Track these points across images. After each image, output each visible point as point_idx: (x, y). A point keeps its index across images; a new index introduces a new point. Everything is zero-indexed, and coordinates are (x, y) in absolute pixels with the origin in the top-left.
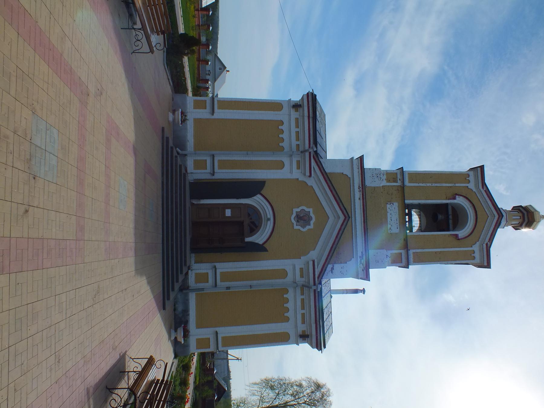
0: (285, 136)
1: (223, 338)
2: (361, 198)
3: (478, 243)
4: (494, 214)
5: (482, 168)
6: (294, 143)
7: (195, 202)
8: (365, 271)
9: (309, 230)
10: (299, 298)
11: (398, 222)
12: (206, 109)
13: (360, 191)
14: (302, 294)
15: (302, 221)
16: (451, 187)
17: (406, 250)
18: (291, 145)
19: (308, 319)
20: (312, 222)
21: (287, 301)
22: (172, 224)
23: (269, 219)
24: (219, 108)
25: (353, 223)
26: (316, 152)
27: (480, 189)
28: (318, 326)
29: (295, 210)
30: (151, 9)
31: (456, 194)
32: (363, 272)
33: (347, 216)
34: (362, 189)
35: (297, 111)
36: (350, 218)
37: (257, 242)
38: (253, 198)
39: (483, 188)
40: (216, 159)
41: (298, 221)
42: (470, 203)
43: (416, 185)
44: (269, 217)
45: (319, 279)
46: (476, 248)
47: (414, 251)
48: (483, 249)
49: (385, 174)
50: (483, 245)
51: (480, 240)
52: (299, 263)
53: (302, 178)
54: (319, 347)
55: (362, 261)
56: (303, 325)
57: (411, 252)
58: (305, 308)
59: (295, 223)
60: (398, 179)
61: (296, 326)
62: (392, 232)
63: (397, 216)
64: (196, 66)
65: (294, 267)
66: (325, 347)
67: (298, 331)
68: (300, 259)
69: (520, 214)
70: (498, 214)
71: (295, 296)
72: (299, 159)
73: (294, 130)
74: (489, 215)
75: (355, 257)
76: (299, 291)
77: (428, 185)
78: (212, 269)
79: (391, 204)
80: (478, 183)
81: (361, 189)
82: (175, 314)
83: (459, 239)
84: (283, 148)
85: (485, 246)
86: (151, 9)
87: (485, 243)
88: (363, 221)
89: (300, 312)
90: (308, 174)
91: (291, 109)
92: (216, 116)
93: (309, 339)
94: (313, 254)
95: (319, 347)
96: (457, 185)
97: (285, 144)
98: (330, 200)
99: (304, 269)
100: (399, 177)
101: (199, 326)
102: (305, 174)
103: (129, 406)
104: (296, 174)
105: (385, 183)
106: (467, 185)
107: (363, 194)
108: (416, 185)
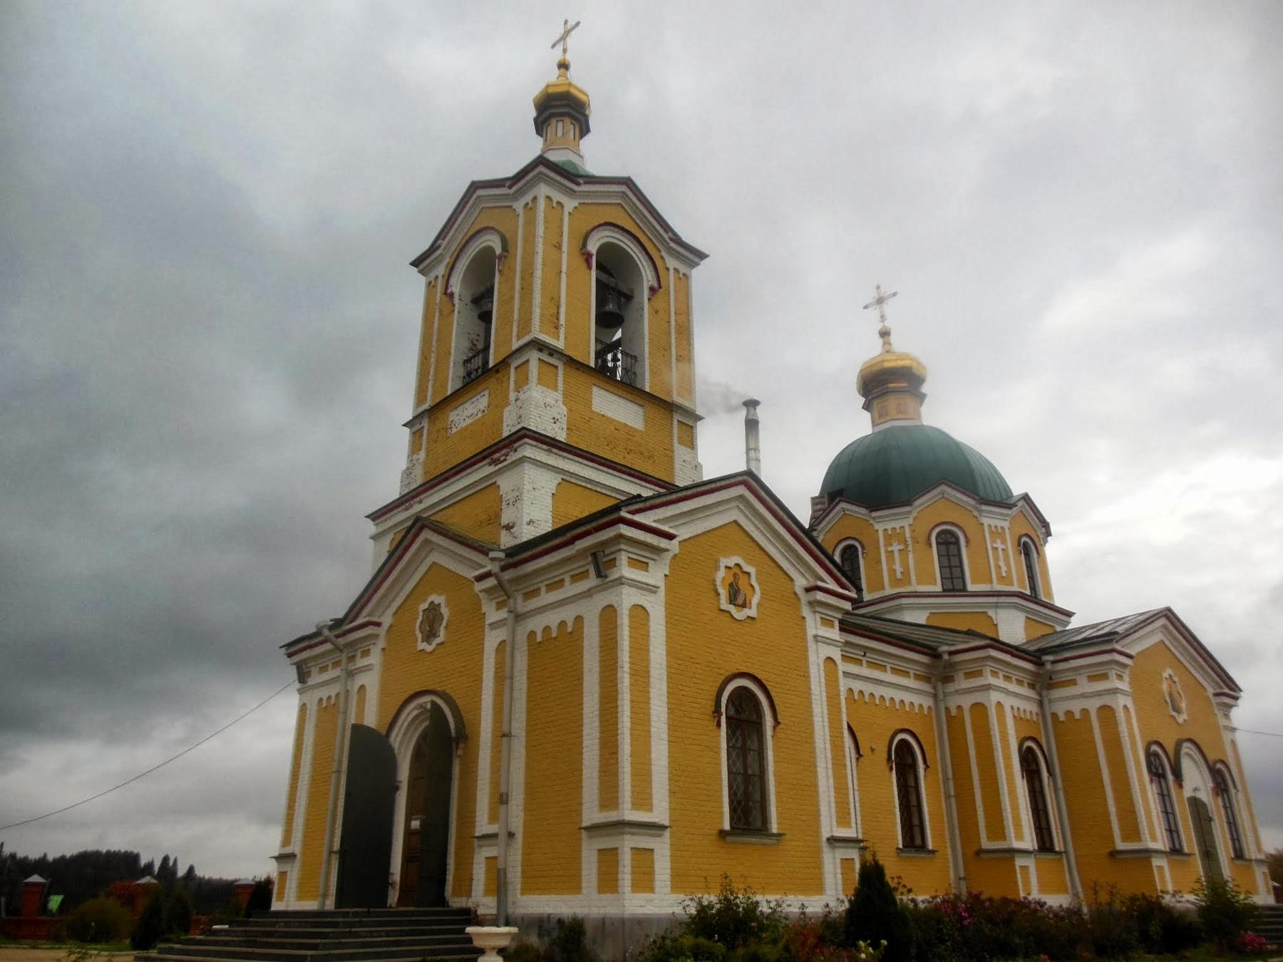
3: (663, 254)
4: (476, 200)
5: (415, 263)
8: (516, 445)
9: (448, 605)
13: (411, 506)
17: (509, 361)
22: (439, 942)
26: (331, 628)
27: (444, 250)
29: (725, 604)
31: (445, 293)
34: (406, 501)
35: (309, 674)
38: (399, 749)
39: (439, 247)
42: (460, 258)
50: (513, 195)
53: (381, 643)
59: (438, 640)
69: (553, 121)
70: (474, 192)
72: (520, 598)
74: (619, 201)
85: (672, 244)
88: (445, 484)
90: (369, 630)
91: (608, 579)
92: (660, 812)
99: (497, 600)
100: (417, 427)
102: (377, 636)
105: (422, 455)
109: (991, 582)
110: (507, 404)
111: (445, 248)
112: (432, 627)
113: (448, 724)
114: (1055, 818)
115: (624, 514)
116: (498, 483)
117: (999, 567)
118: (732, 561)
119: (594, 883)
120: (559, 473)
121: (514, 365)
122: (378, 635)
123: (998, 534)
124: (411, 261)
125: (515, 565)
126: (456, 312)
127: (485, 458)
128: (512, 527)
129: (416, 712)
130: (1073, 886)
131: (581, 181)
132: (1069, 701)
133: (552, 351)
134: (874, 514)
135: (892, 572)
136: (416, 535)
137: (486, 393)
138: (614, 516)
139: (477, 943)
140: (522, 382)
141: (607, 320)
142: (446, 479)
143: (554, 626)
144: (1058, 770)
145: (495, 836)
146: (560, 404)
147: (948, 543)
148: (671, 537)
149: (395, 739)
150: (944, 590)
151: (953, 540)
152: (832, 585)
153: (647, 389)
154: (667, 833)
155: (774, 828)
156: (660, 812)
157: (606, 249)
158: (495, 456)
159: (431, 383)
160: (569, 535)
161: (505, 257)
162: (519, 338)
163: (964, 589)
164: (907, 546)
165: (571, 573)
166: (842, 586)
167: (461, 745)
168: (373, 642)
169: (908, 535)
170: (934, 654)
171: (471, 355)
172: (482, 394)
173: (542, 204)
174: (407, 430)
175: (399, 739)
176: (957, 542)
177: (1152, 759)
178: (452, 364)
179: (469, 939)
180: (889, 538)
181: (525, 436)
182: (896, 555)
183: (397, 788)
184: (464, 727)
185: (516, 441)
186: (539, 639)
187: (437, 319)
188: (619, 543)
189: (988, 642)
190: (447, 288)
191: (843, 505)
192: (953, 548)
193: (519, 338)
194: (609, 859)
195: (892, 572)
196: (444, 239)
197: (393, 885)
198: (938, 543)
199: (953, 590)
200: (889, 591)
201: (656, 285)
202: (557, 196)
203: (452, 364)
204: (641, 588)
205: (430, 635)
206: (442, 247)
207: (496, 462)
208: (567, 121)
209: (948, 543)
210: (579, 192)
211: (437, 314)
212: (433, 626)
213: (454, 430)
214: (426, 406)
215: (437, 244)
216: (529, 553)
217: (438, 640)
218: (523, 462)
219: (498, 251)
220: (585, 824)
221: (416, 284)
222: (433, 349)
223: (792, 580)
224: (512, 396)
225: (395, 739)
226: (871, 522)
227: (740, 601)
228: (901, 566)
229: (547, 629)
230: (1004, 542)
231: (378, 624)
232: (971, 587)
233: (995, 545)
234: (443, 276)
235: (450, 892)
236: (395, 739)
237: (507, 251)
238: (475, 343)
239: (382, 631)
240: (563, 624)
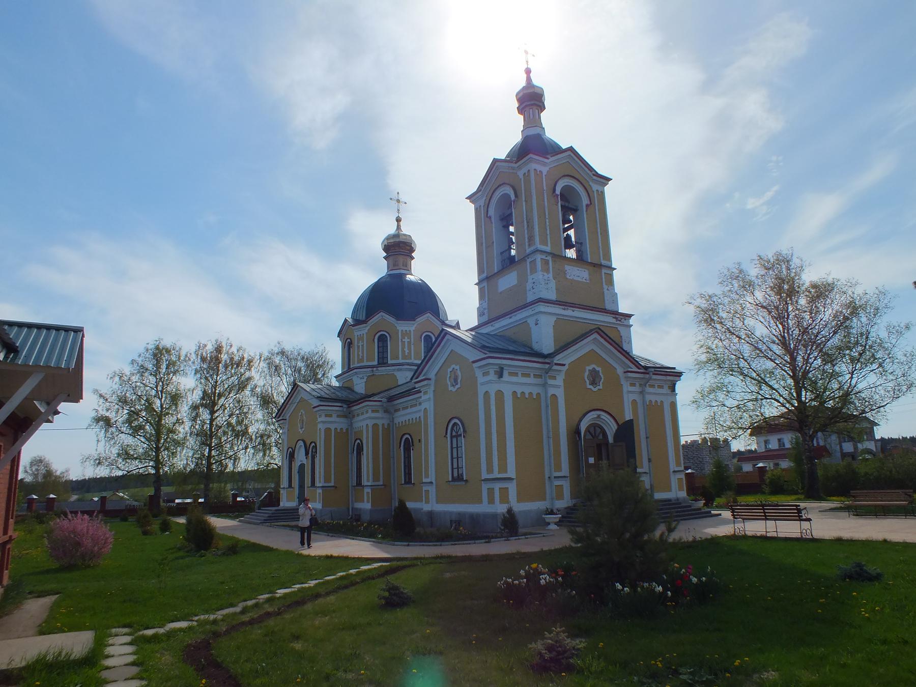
0: (527, 391)
2: (574, 309)
3: (591, 183)
6: (531, 380)
11: (580, 269)
12: (508, 488)
18: (530, 384)
20: (597, 369)
23: (599, 416)
24: (506, 472)
25: (593, 323)
28: (671, 374)
30: (769, 516)
32: (575, 312)
33: (595, 331)
34: (566, 306)
36: (601, 327)
37: (614, 430)
40: (424, 480)
41: (596, 384)
43: (549, 237)
44: (595, 416)
45: (640, 367)
46: (595, 187)
47: (527, 247)
49: (542, 273)
52: (626, 387)
53: (432, 388)
54: (681, 374)
56: (557, 378)
57: (604, 262)
60: (546, 258)
61: (667, 394)
62: (588, 279)
63: (576, 268)
64: (130, 523)
65: (629, 392)
66: (674, 368)
67: (494, 379)
68: (622, 385)
73: (520, 379)
75: (616, 326)
77: (548, 224)
78: (675, 475)
79: (566, 272)
81: (566, 307)
83: (591, 204)
84: (538, 394)
85: (594, 177)
86: (769, 516)
87: (592, 176)
88: (591, 312)
90: (425, 382)
92: (513, 476)
93: (505, 368)
94: (620, 371)
95: (681, 374)
96: (545, 188)
97: (535, 391)
100: (482, 286)
103: (79, 686)
104: (560, 381)
105: (551, 275)
106: (544, 177)
108: (549, 237)
114: (320, 475)
116: (528, 322)
118: (590, 368)
119: (434, 499)
121: (529, 261)
122: (430, 384)
123: (406, 334)
128: (428, 338)
132: (402, 417)
134: (399, 322)
135: (403, 351)
140: (534, 270)
143: (659, 402)
147: (382, 340)
153: (589, 261)
154: (515, 481)
156: (511, 472)
158: (617, 316)
162: (547, 246)
168: (558, 373)
173: (532, 174)
180: (404, 335)
182: (406, 343)
191: (382, 313)
194: (491, 492)
195: (403, 351)
196: (482, 187)
200: (401, 361)
201: (589, 203)
202: (539, 167)
208: (535, 107)
214: (485, 275)
219: (513, 197)
220: (483, 478)
221: (471, 207)
223: (616, 369)
226: (396, 325)
228: (408, 350)
230: (363, 342)
231: (430, 379)
233: (403, 340)
234: (484, 206)
239: (432, 382)
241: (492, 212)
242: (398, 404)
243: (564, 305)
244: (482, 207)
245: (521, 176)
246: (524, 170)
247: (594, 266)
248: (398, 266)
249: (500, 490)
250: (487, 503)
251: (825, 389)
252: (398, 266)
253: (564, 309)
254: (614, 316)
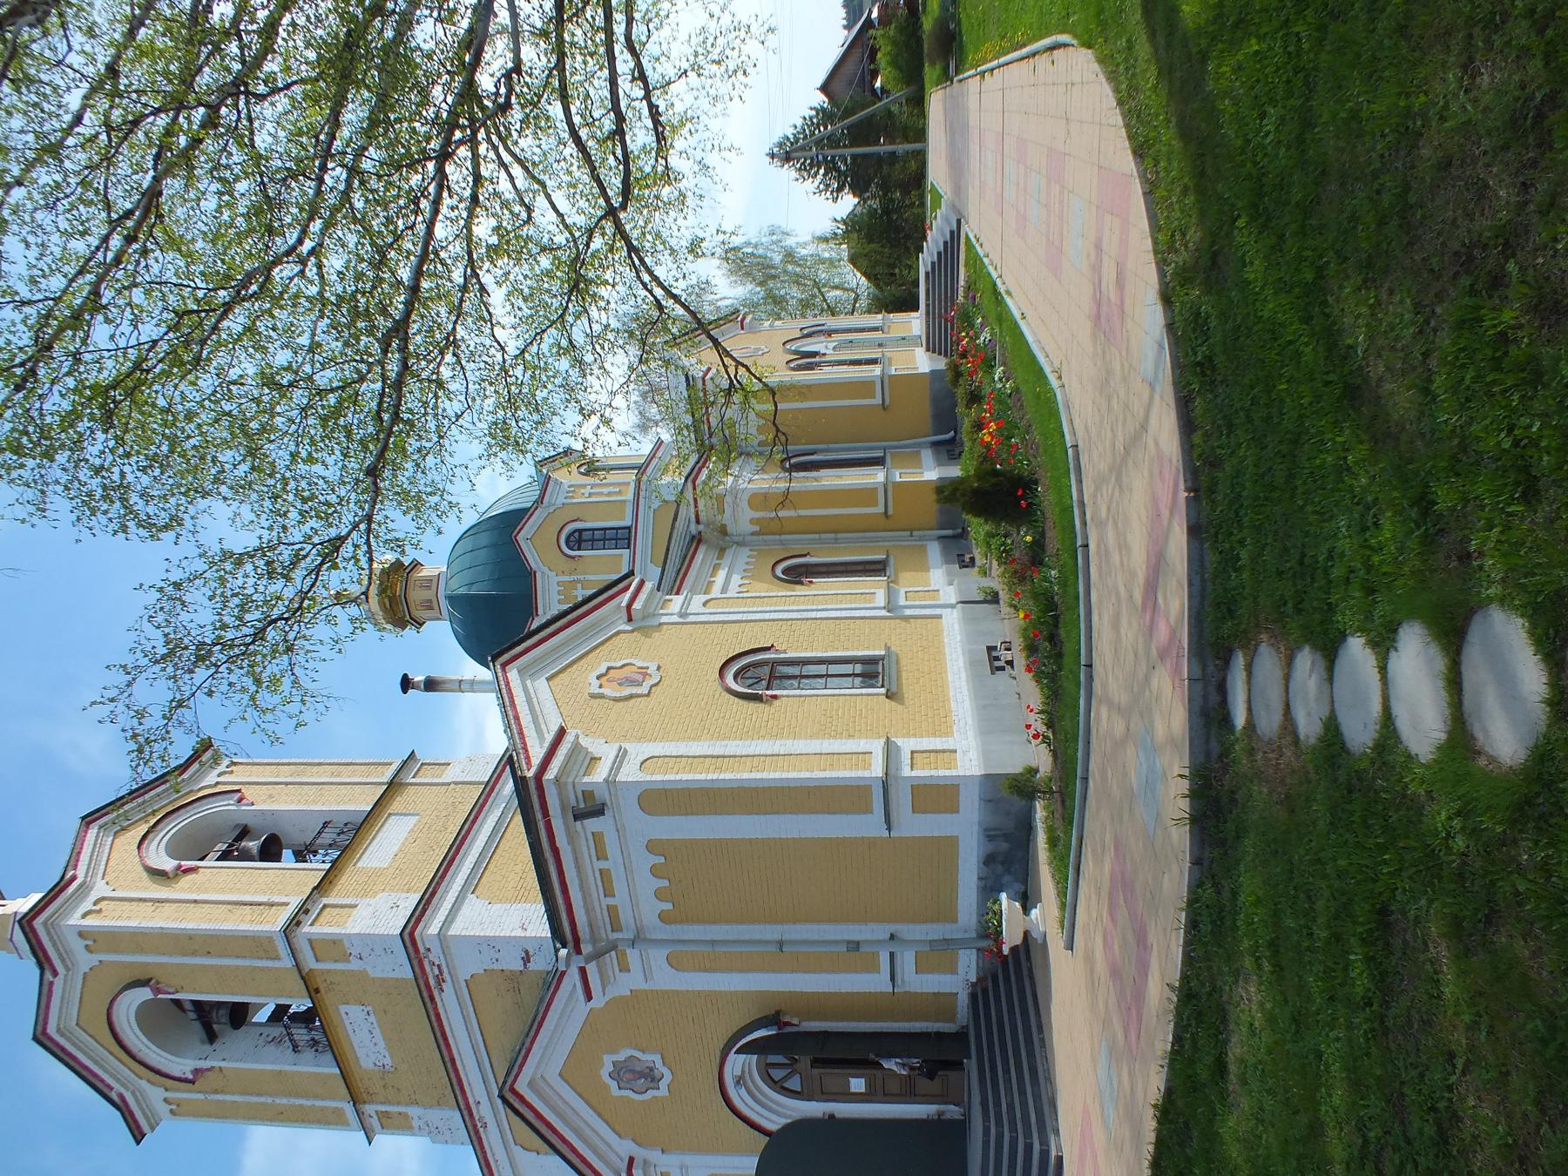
1: (868, 810)
4: (62, 1035)
7: (953, 1111)
8: (422, 950)
9: (606, 1087)
10: (620, 899)
11: (349, 1028)
14: (612, 911)
15: (638, 1069)
16: (216, 1092)
19: (584, 849)
21: (659, 895)
27: (127, 1089)
31: (192, 1082)
34: (475, 1126)
38: (785, 1117)
39: (121, 1097)
47: (277, 964)
48: (63, 961)
50: (68, 969)
51: (81, 977)
53: (654, 1156)
55: (437, 972)
58: (598, 875)
59: (659, 1064)
63: (355, 1040)
71: (634, 905)
76: (625, 916)
80: (137, 1100)
81: (479, 1125)
82: (1025, 882)
89: (614, 863)
91: (608, 802)
98: (576, 860)
99: (617, 970)
100: (375, 1122)
101: (951, 843)
105: (413, 1111)
107: (471, 1115)
108: (319, 1103)
109: (625, 501)
110: (364, 973)
111: (123, 1085)
112: (642, 1075)
113: (762, 1038)
115: (530, 774)
117: (609, 494)
120: (464, 898)
124: (134, 1143)
125: (577, 941)
126: (223, 1064)
127: (432, 998)
128: (527, 952)
129: (743, 1091)
130: (914, 445)
131: (70, 874)
133: (303, 909)
136: (521, 1098)
137: (343, 1009)
138: (532, 786)
139: (1018, 940)
141: (271, 851)
142: (453, 1060)
144: (812, 447)
145: (892, 955)
146: (372, 901)
147: (579, 539)
148: (562, 733)
149: (774, 1123)
150: (629, 547)
151: (577, 534)
152: (627, 596)
155: (883, 653)
157: (173, 852)
158: (432, 982)
159: (319, 1103)
160: (548, 854)
161: (158, 983)
162: (277, 958)
163: (629, 528)
164: (579, 581)
165: (594, 859)
166: (627, 588)
167: (787, 1019)
169: (567, 578)
170: (697, 540)
171: (288, 1043)
172: (344, 1016)
174: (379, 1139)
175: (774, 1117)
176: (580, 531)
177: (799, 368)
178: (295, 1068)
179: (1014, 949)
181: (412, 934)
183: (832, 1117)
184: (766, 1017)
185: (417, 950)
186: (668, 906)
187: (228, 1098)
188: (566, 783)
189: (690, 485)
190: (186, 1081)
192: (586, 535)
193: (277, 958)
197: (940, 1114)
198: (579, 549)
199: (629, 539)
203: (295, 1068)
204: (621, 763)
205: (651, 1077)
206: (122, 1090)
207: (440, 980)
209: (579, 539)
210: (86, 877)
211: (220, 1097)
212: (639, 1072)
213: (388, 1061)
214: (348, 1108)
215: (116, 1099)
216: (564, 916)
217: (659, 1064)
218: (445, 936)
219: (145, 994)
222: (269, 1100)
224: (355, 965)
225: (774, 1122)
227: (640, 678)
229: (659, 895)
232: (627, 522)
235: (951, 1025)
236: (774, 1122)
237: (151, 979)
238: (270, 1039)
240: (655, 871)
241: (181, 1066)
242: (590, 925)
243: (477, 1132)
244: (169, 1095)
245: (94, 959)
246: (77, 945)
247: (317, 991)
248: (430, 601)
249: (923, 972)
250: (869, 815)
251: (1409, 135)
252: (430, 601)
253: (485, 1126)
254: (436, 993)
